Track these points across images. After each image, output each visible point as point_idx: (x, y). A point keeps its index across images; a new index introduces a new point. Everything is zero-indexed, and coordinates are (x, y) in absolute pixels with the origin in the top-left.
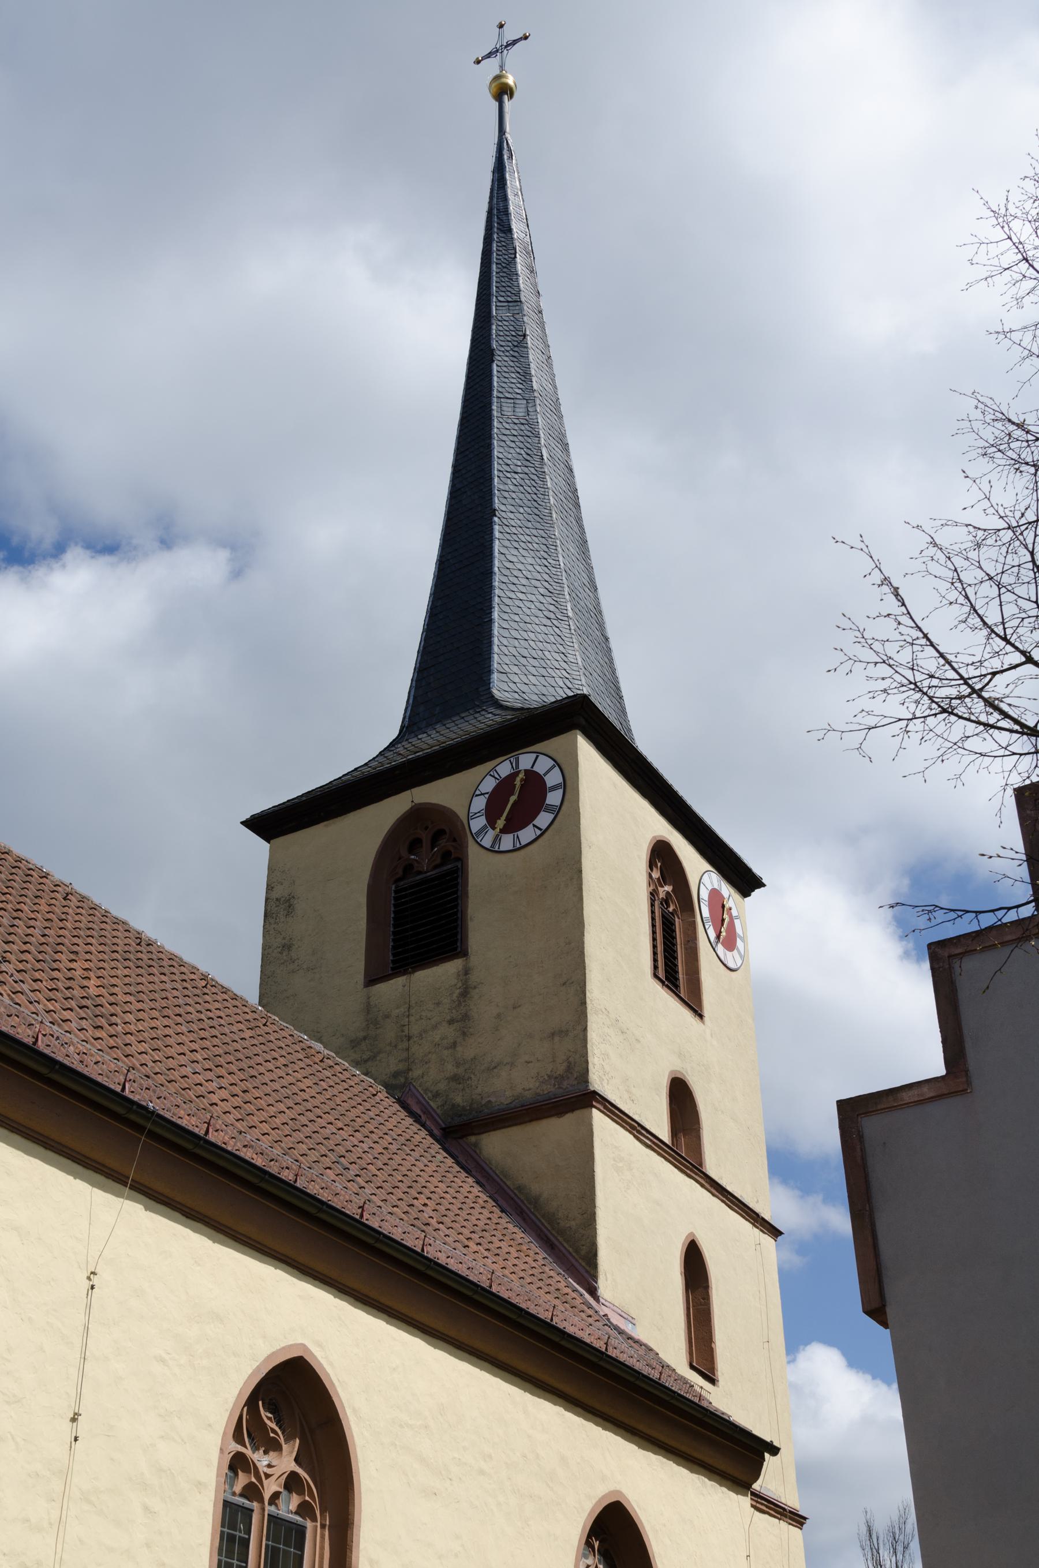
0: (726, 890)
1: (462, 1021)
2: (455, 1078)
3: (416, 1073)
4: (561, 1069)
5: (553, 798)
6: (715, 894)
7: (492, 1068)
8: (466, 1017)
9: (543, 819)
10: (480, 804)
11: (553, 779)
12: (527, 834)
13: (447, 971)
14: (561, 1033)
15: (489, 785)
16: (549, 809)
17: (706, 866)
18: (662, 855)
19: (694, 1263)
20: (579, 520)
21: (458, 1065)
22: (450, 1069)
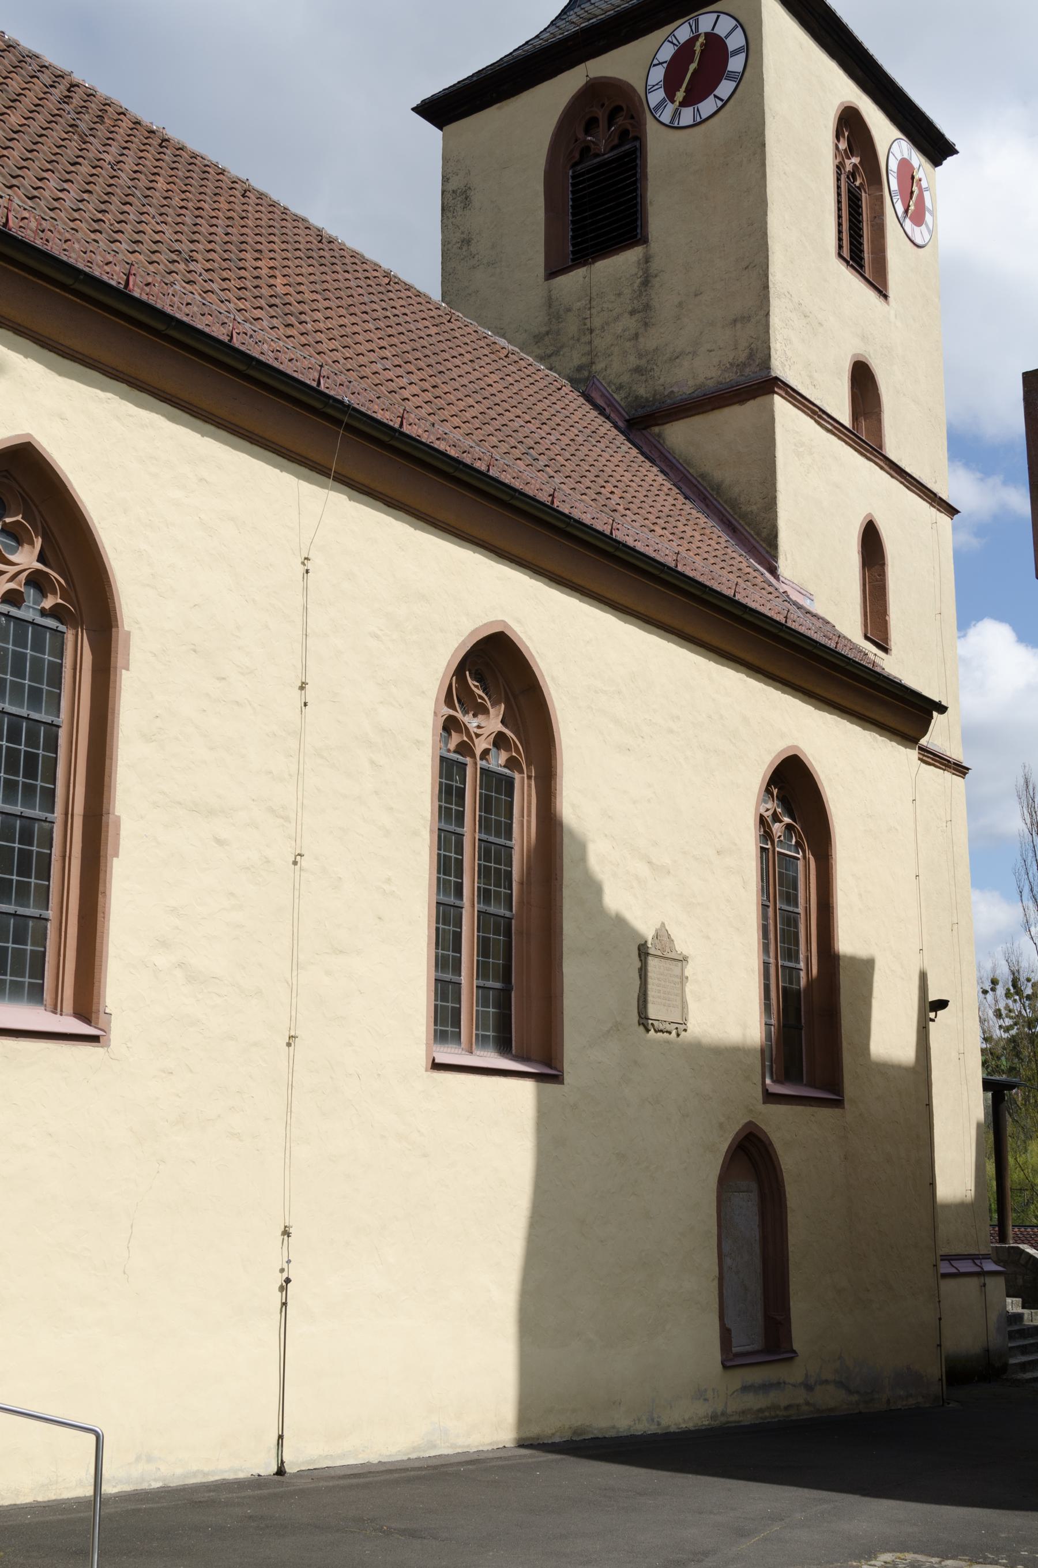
0: (917, 159)
1: (644, 312)
2: (638, 370)
3: (599, 366)
4: (743, 357)
5: (735, 64)
6: (904, 164)
7: (675, 358)
8: (647, 307)
9: (725, 88)
10: (658, 75)
11: (735, 41)
12: (707, 106)
13: (626, 260)
14: (741, 319)
15: (667, 53)
16: (736, 52)
17: (896, 133)
18: (850, 122)
19: (871, 543)
20: (382, 1472)
21: (640, 356)
22: (633, 361)
